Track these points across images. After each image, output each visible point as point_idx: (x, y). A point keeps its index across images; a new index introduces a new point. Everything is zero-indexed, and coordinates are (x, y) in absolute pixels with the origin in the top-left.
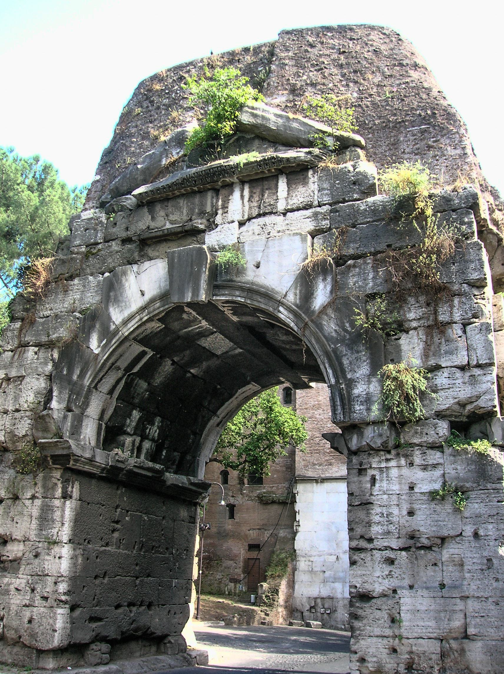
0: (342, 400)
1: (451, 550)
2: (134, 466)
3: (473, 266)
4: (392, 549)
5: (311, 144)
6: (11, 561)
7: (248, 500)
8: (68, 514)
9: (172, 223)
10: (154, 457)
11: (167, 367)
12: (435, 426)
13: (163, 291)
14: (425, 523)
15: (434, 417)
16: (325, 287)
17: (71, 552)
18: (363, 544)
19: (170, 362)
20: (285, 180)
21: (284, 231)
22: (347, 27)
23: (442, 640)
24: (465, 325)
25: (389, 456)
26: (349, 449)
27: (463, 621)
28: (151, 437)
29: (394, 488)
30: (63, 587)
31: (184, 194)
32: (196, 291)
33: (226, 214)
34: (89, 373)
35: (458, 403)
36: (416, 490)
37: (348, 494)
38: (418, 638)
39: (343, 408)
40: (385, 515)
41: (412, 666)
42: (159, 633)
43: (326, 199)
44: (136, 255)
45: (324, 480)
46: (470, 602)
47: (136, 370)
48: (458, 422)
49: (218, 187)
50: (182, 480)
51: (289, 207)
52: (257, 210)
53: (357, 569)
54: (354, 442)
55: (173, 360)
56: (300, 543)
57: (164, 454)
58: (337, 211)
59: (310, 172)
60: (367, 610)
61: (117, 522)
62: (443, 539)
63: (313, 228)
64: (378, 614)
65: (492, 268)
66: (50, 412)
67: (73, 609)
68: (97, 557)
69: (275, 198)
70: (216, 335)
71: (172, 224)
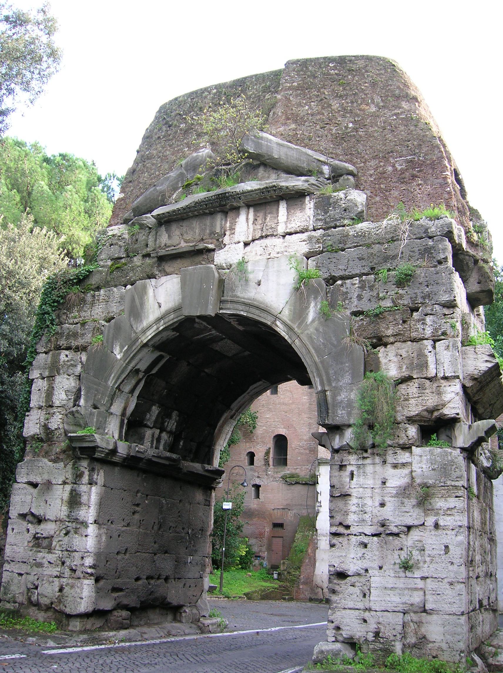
1: (415, 537)
2: (153, 456)
4: (366, 535)
5: (309, 173)
6: (45, 538)
7: (273, 481)
9: (186, 241)
10: (172, 448)
11: (183, 367)
13: (177, 304)
15: (406, 422)
16: (316, 304)
17: (96, 531)
18: (341, 530)
19: (185, 364)
20: (285, 205)
21: (282, 252)
22: (348, 58)
23: (404, 614)
24: (435, 341)
25: (365, 455)
27: (423, 598)
28: (169, 429)
29: (369, 482)
30: (89, 561)
31: (197, 215)
33: (233, 236)
34: (113, 375)
35: (426, 410)
36: (388, 484)
37: (331, 486)
38: (385, 611)
40: (360, 506)
41: (379, 635)
42: (175, 603)
47: (154, 371)
48: (426, 425)
49: (226, 210)
50: (197, 467)
51: (288, 231)
52: (260, 232)
53: (335, 551)
55: (188, 362)
57: (181, 443)
58: (329, 236)
59: (308, 198)
60: (343, 585)
61: (138, 505)
62: (409, 528)
63: (307, 250)
66: (79, 408)
67: (97, 580)
68: (119, 536)
69: (276, 221)
70: (226, 340)
71: (186, 242)
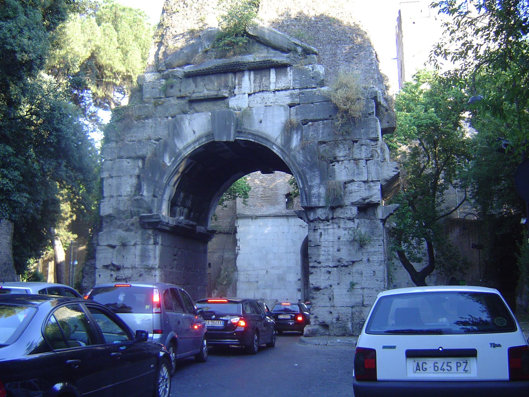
0: (306, 195)
3: (372, 130)
5: (288, 51)
8: (158, 253)
9: (208, 90)
12: (351, 209)
14: (345, 255)
16: (297, 137)
20: (274, 72)
25: (328, 223)
26: (308, 219)
32: (229, 136)
34: (165, 176)
35: (362, 199)
36: (341, 239)
39: (306, 200)
43: (297, 86)
44: (187, 108)
45: (257, 217)
46: (365, 290)
54: (312, 216)
56: (240, 262)
59: (289, 69)
63: (290, 102)
64: (323, 296)
65: (381, 125)
